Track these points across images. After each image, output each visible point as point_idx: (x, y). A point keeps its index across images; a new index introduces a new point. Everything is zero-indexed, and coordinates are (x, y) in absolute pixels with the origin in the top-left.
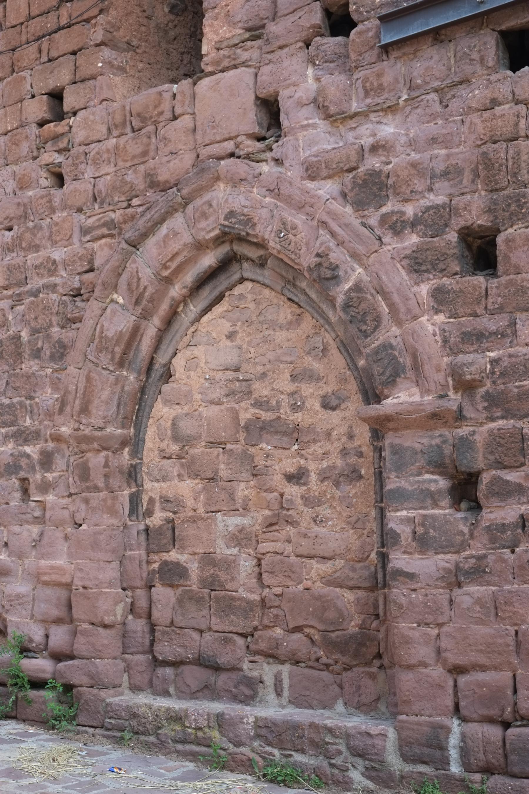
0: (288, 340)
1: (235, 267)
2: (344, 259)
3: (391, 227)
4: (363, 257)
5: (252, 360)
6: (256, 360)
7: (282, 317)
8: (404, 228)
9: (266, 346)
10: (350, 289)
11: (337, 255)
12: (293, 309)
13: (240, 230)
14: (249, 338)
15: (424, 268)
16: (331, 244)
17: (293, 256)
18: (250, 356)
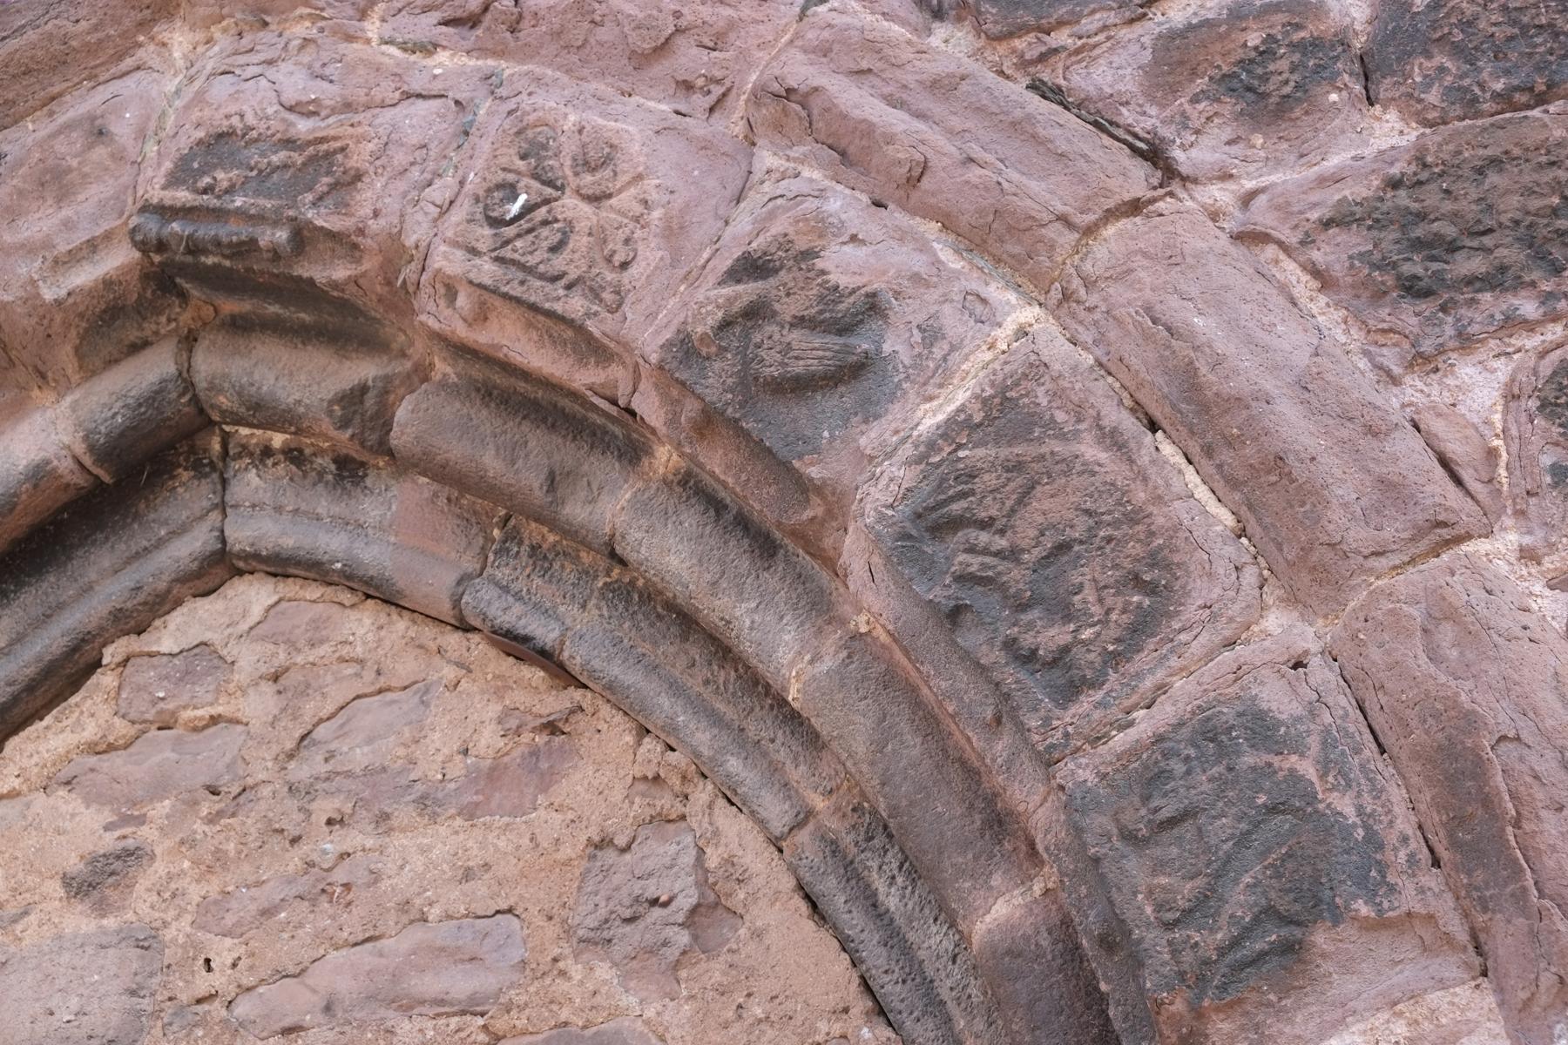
0: (468, 875)
1: (188, 497)
2: (919, 263)
3: (1228, 84)
4: (1054, 232)
5: (216, 1009)
6: (243, 1008)
7: (440, 742)
8: (1324, 74)
9: (323, 917)
10: (958, 428)
11: (866, 249)
12: (518, 698)
13: (259, 218)
14: (213, 887)
15: (1473, 265)
16: (833, 205)
17: (575, 305)
18: (203, 983)
